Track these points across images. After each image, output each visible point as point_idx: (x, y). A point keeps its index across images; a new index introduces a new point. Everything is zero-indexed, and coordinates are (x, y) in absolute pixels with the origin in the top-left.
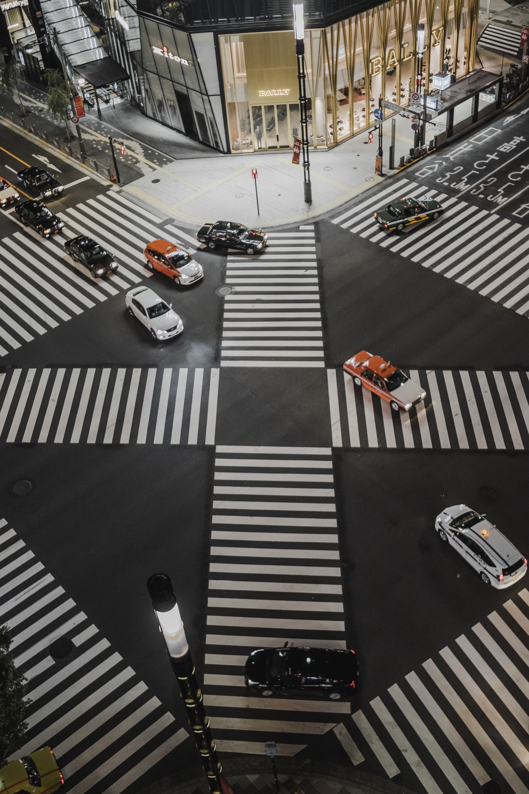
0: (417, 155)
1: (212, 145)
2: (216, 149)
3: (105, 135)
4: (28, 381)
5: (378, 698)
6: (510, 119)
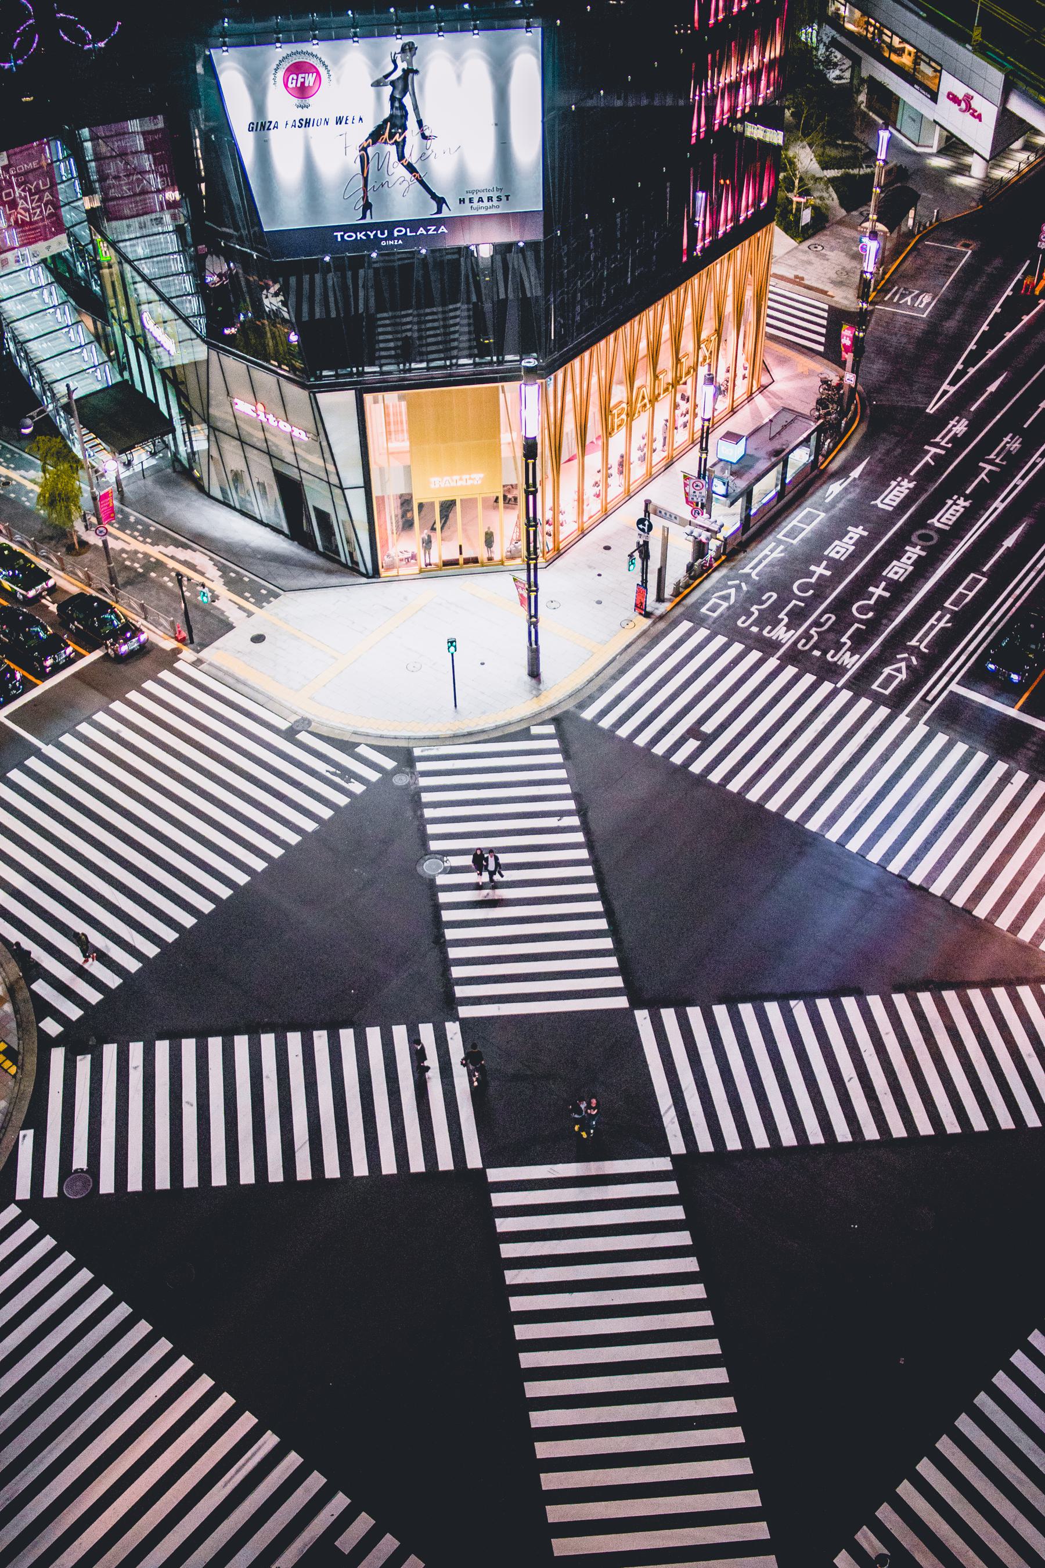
0: (696, 573)
1: (343, 559)
2: (353, 568)
3: (141, 539)
4: (135, 1068)
5: (536, 1444)
6: (835, 488)
